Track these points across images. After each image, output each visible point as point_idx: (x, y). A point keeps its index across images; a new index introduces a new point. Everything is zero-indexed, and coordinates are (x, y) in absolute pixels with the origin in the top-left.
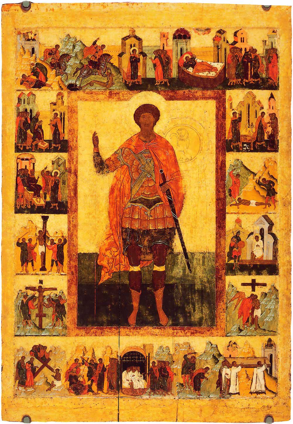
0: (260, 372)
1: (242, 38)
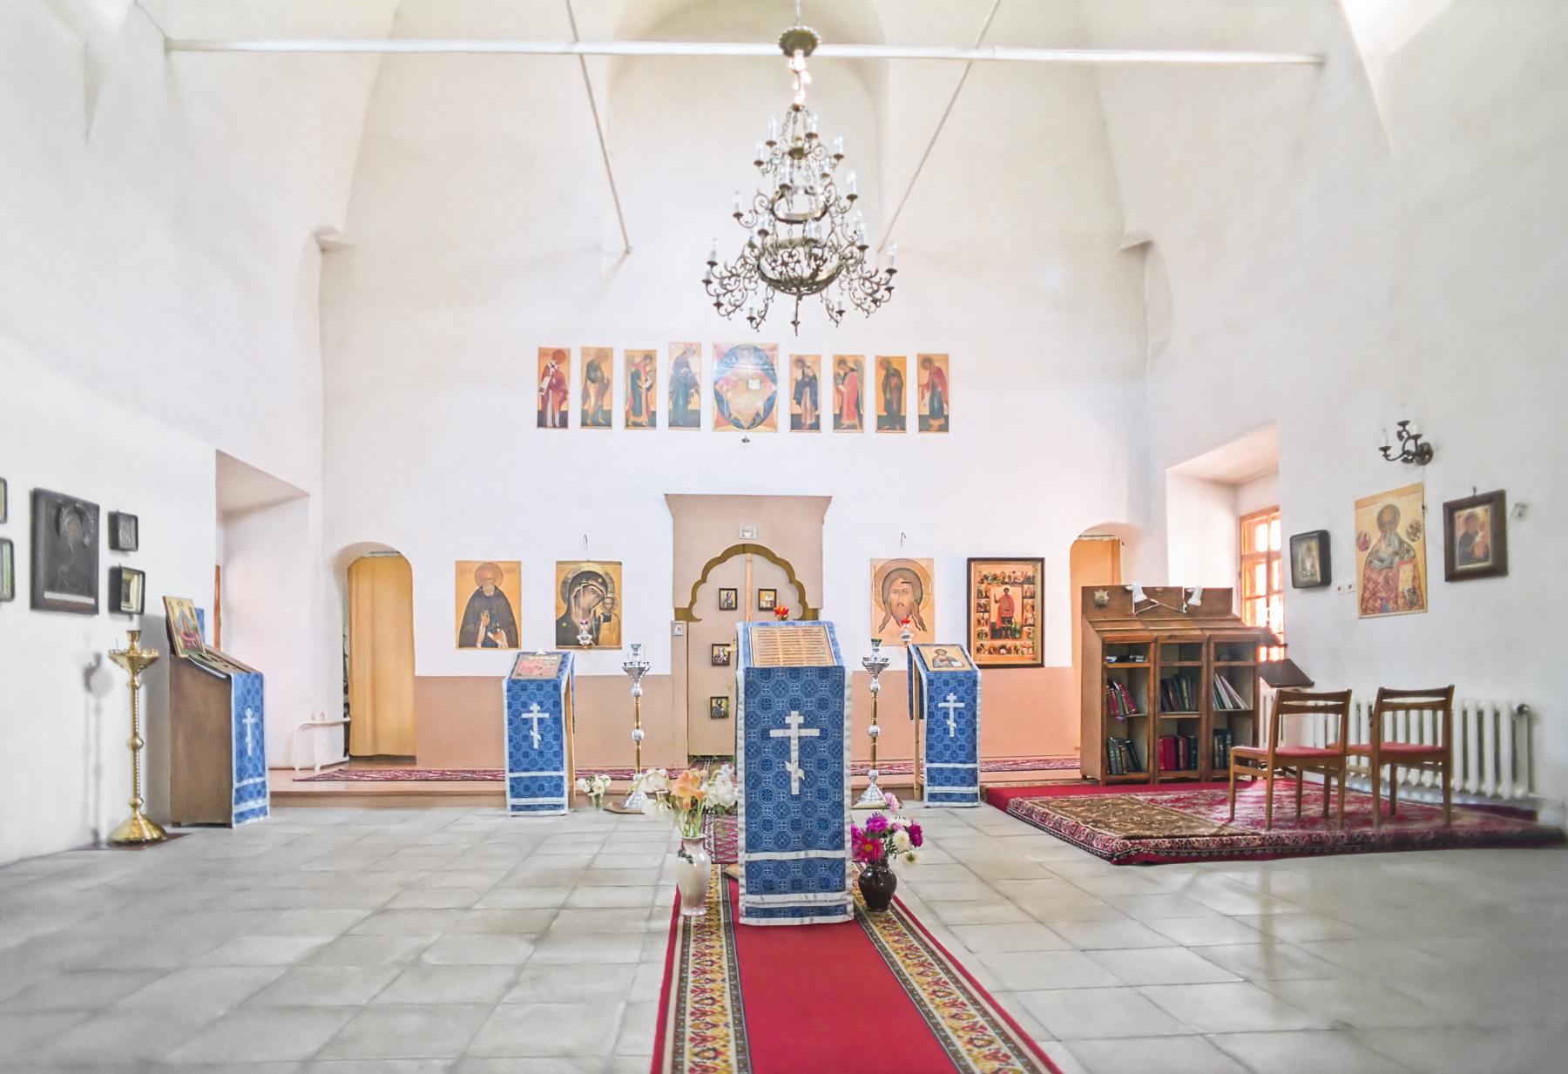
1: (913, 378)
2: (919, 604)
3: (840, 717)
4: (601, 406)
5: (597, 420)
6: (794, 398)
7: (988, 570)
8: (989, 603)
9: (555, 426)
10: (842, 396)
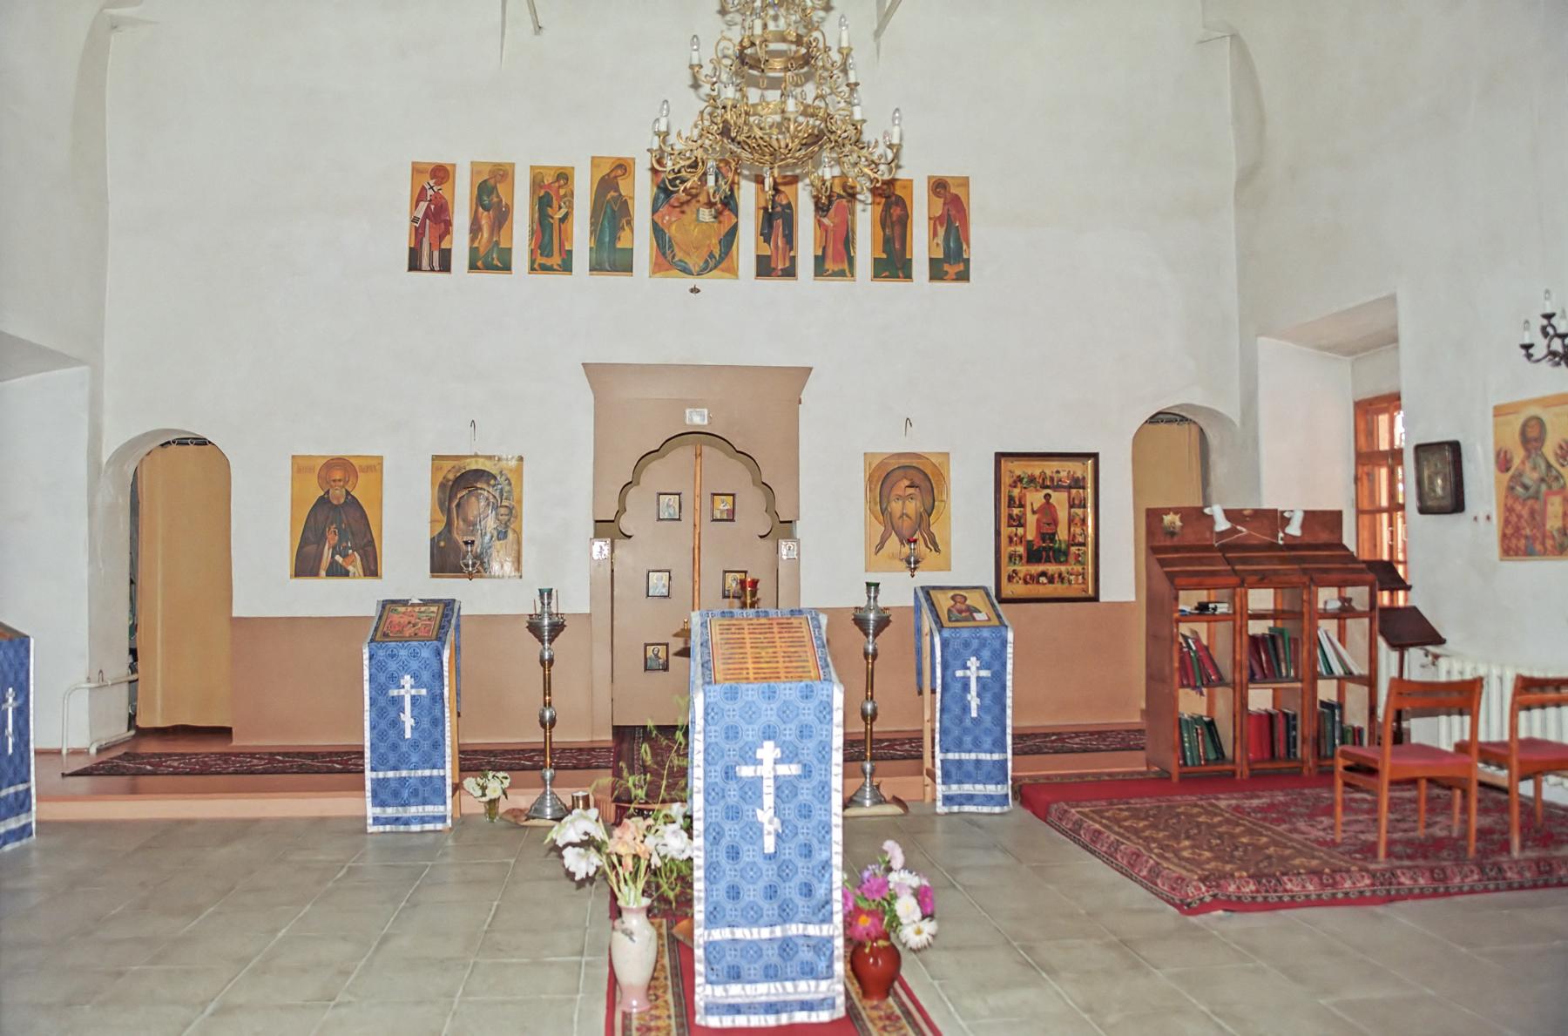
0: (1080, 577)
2: (929, 515)
3: (827, 749)
4: (497, 243)
5: (490, 260)
6: (761, 235)
7: (1019, 468)
8: (1025, 514)
9: (432, 270)
10: (826, 231)
